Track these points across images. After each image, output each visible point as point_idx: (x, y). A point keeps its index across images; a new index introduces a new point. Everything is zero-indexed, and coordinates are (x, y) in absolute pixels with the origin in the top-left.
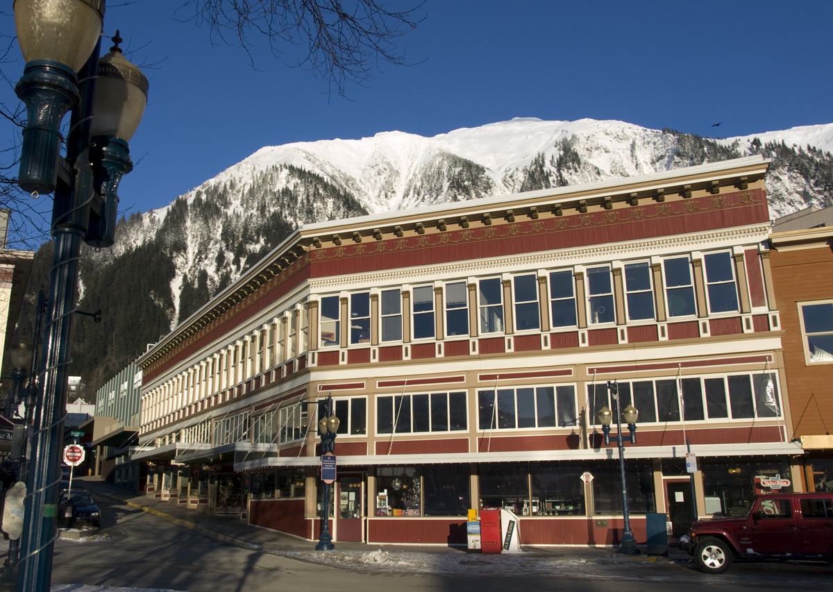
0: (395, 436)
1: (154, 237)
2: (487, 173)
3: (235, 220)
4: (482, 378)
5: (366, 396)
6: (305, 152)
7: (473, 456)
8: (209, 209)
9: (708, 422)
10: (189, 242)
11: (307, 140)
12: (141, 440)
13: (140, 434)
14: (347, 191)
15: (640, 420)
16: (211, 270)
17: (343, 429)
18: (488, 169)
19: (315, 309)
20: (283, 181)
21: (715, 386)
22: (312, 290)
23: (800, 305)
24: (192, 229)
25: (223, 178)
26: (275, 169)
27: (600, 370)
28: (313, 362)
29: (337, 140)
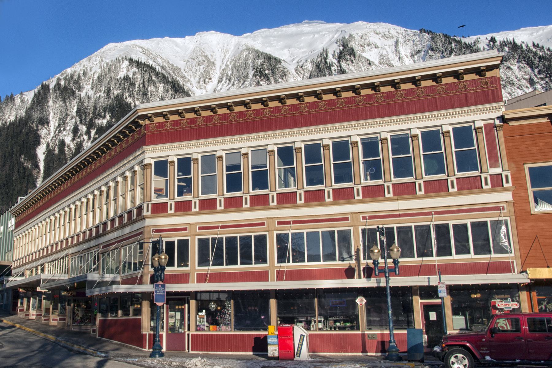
0: (211, 268)
1: (24, 114)
2: (283, 64)
3: (87, 100)
4: (279, 223)
5: (189, 238)
6: (141, 48)
7: (273, 284)
8: (66, 92)
9: (435, 259)
10: (51, 118)
11: (143, 39)
12: (14, 272)
13: (13, 267)
14: (174, 78)
15: (402, 256)
16: (68, 140)
17: (171, 263)
18: (284, 61)
19: (149, 170)
20: (124, 70)
21: (461, 230)
22: (147, 155)
23: (527, 167)
24: (53, 107)
25: (77, 68)
26: (118, 61)
27: (370, 217)
28: (148, 211)
29: (167, 38)
